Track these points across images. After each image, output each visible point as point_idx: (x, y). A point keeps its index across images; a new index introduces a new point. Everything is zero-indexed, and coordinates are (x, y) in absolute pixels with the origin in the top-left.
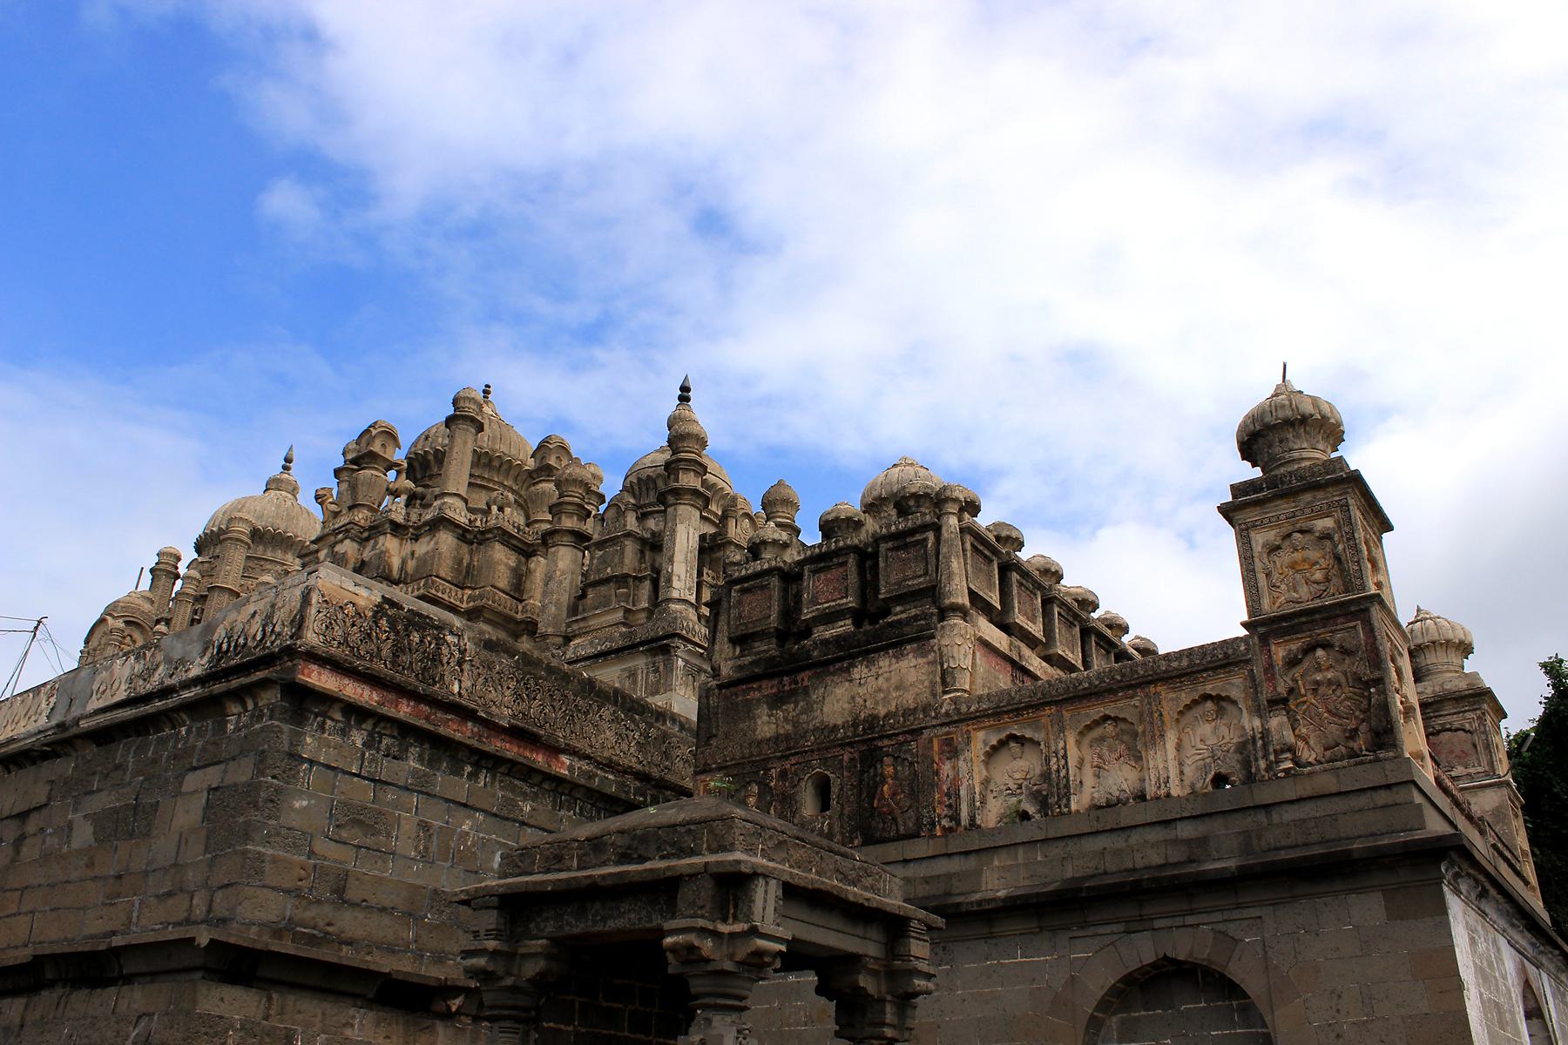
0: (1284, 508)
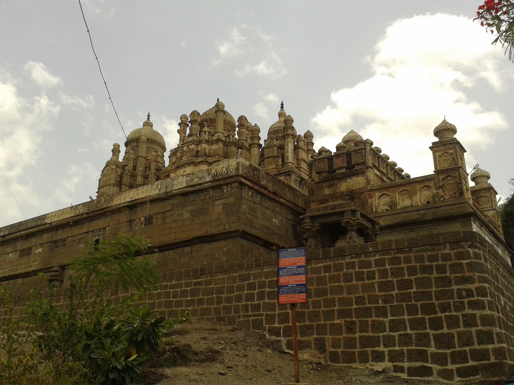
0: (443, 148)
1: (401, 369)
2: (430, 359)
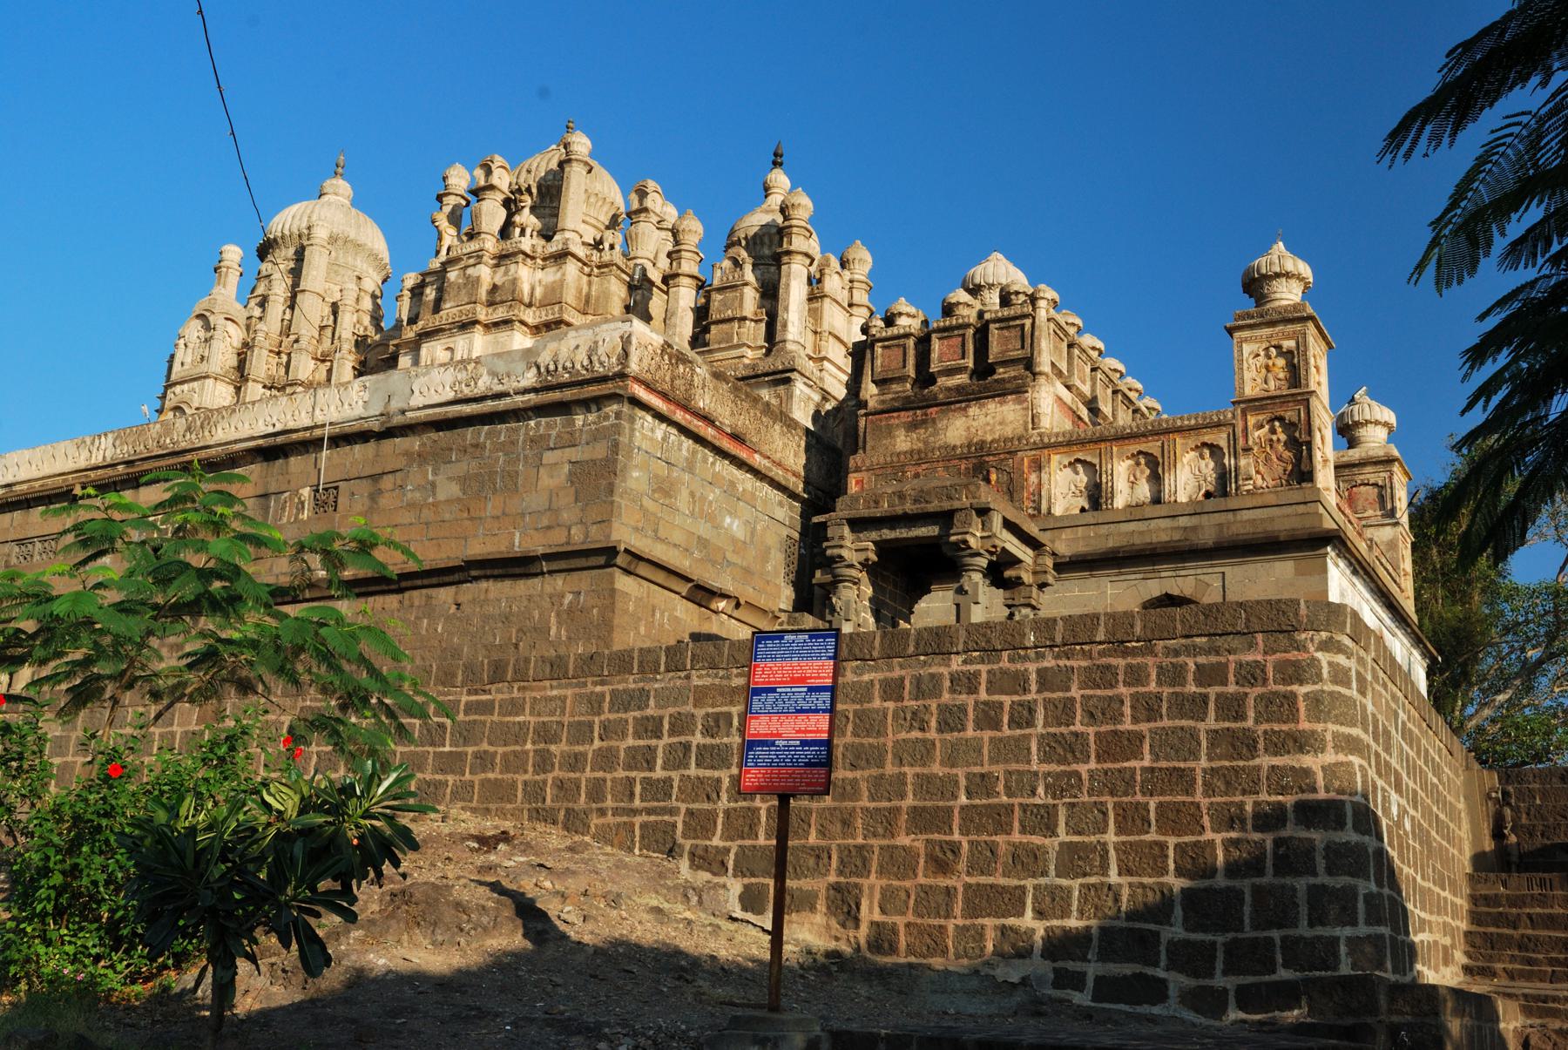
1: (1077, 981)
2: (1163, 956)
